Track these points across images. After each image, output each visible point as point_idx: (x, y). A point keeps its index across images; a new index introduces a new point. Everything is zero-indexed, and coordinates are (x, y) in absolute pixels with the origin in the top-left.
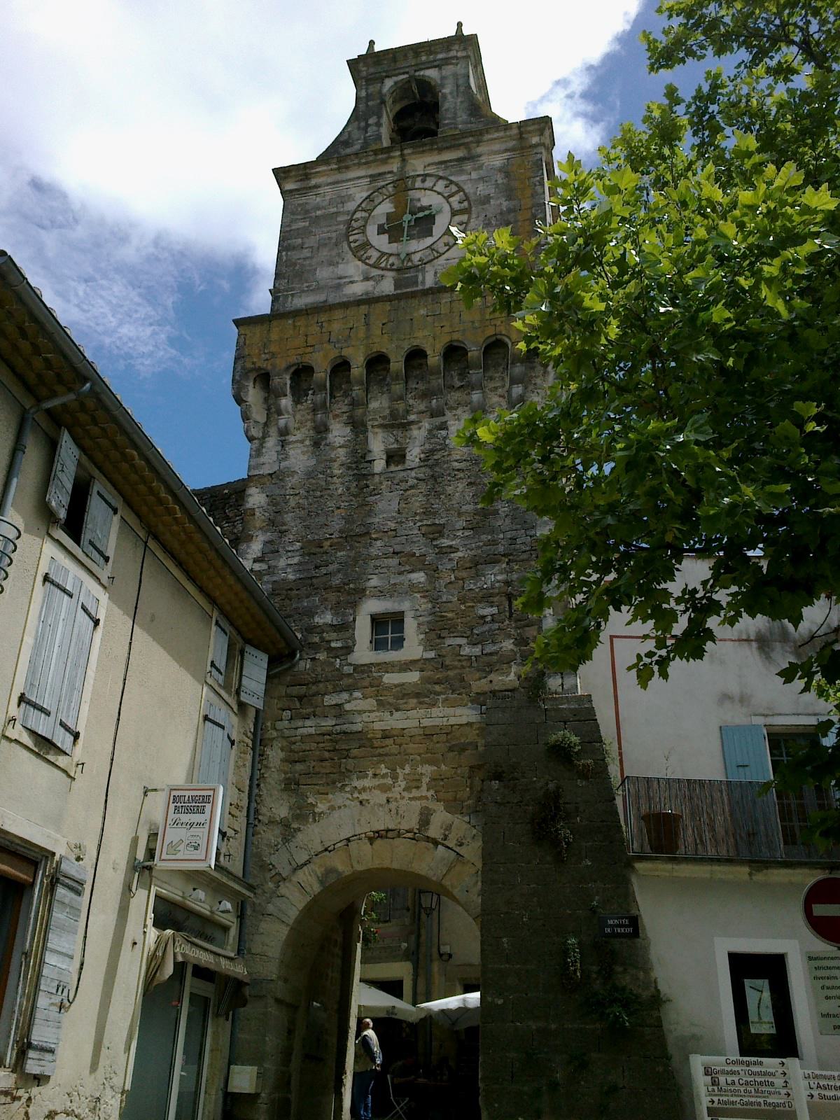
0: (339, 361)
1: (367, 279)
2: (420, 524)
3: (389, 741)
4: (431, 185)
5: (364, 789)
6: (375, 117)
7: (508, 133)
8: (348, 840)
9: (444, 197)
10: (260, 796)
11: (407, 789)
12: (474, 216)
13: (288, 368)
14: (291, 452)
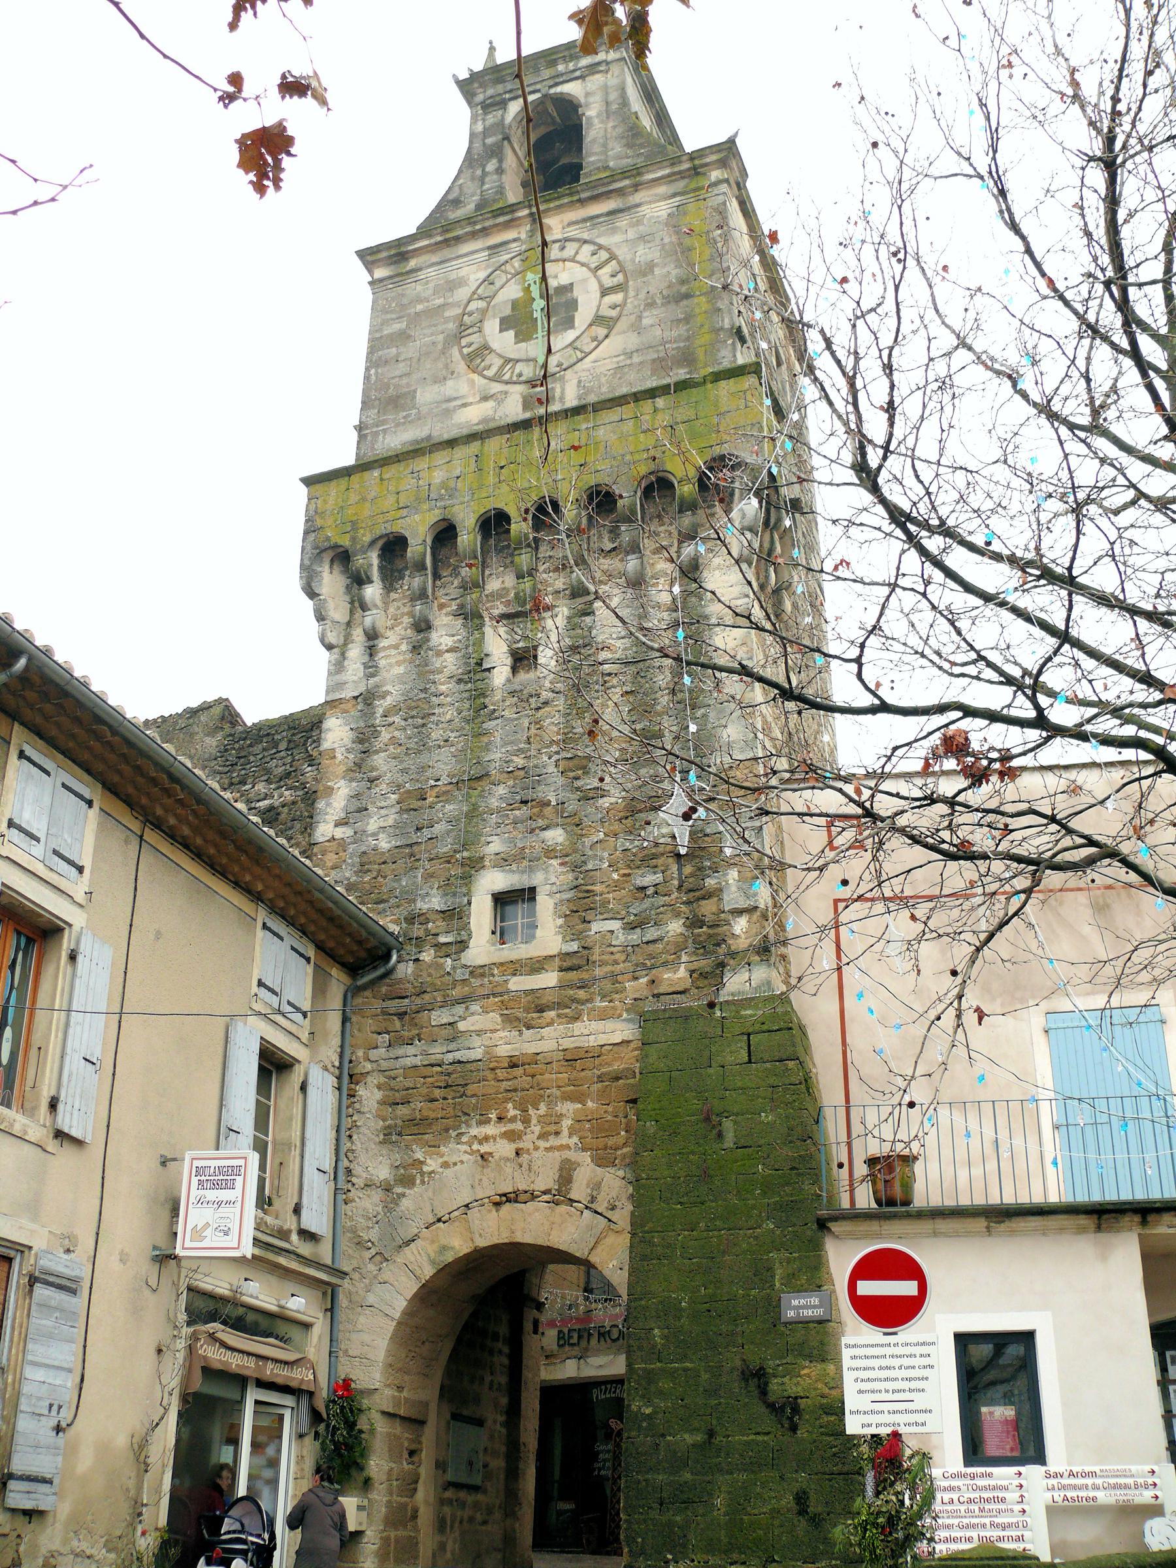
0: (444, 525)
1: (485, 398)
2: (556, 757)
3: (519, 1071)
4: (572, 253)
5: (486, 1139)
6: (494, 161)
7: (676, 169)
8: (467, 1206)
9: (590, 269)
10: (353, 1151)
11: (543, 1136)
12: (631, 293)
13: (373, 543)
14: (382, 663)
